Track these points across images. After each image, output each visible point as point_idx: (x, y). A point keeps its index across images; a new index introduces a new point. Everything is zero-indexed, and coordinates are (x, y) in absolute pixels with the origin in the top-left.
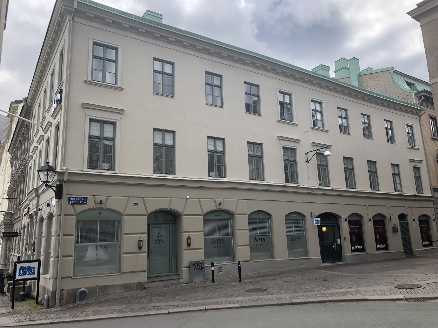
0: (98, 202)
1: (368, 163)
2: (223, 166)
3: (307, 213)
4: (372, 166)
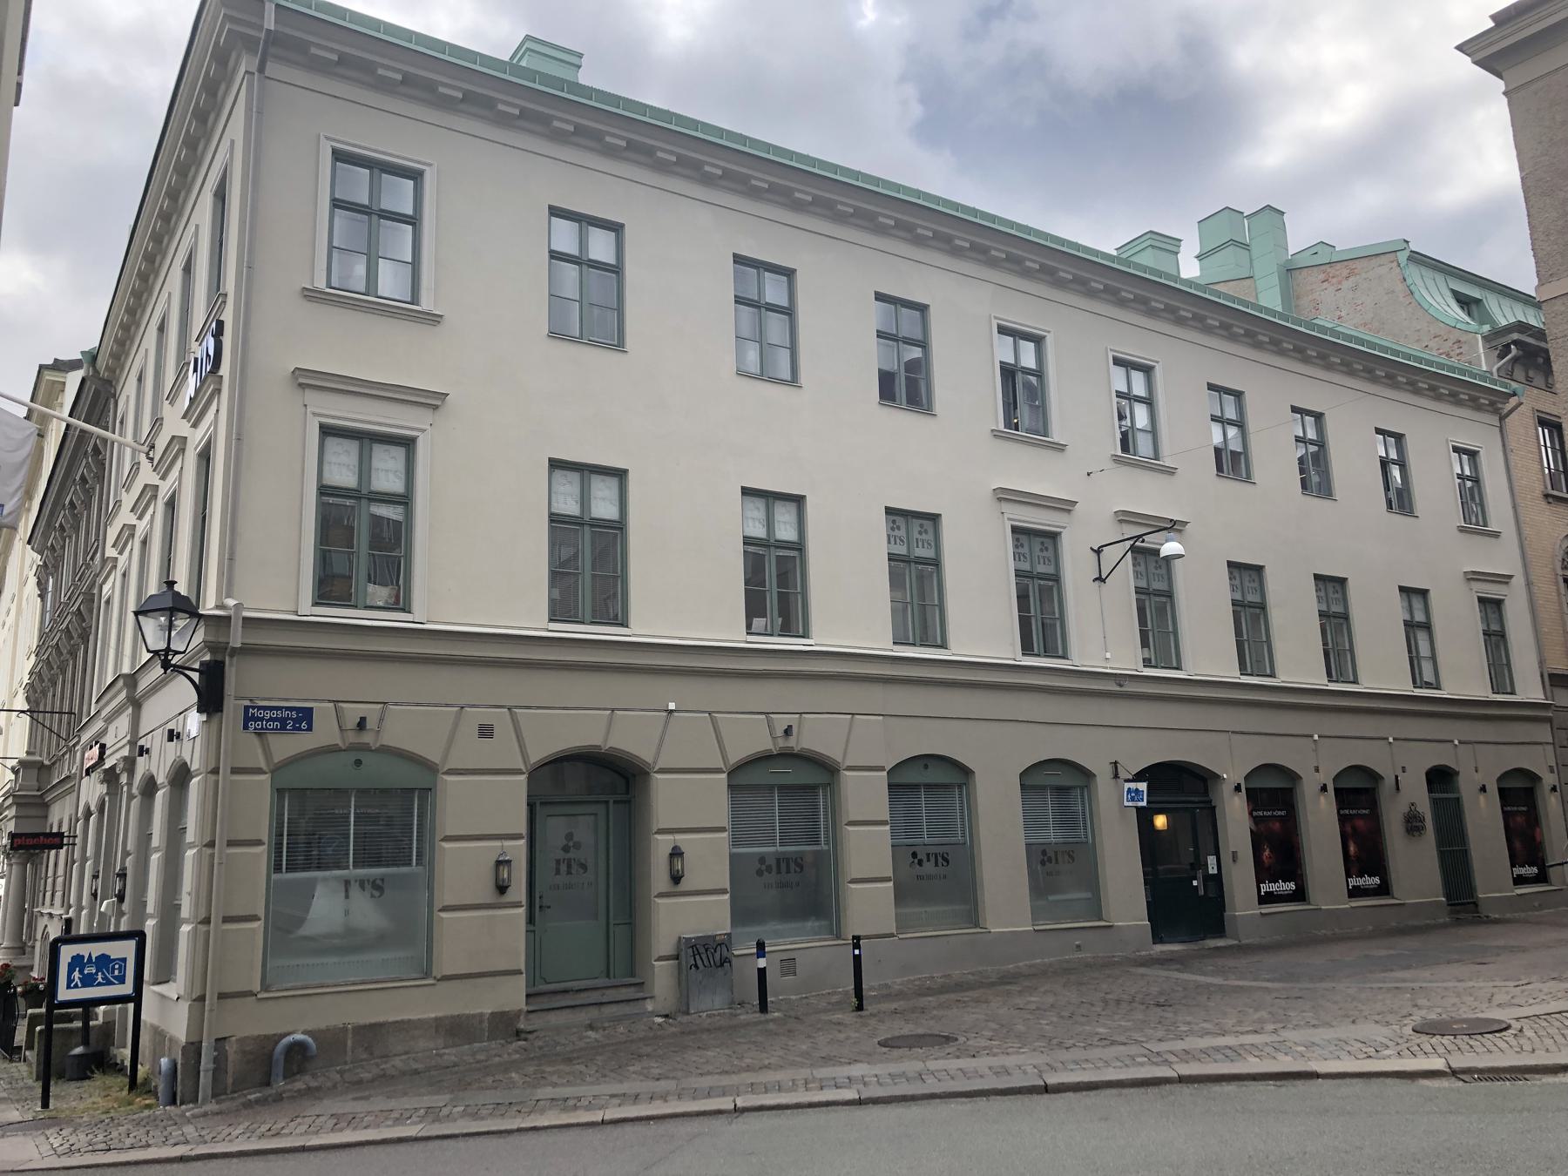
0: (351, 723)
1: (1316, 585)
2: (799, 597)
3: (1098, 765)
4: (1331, 595)
